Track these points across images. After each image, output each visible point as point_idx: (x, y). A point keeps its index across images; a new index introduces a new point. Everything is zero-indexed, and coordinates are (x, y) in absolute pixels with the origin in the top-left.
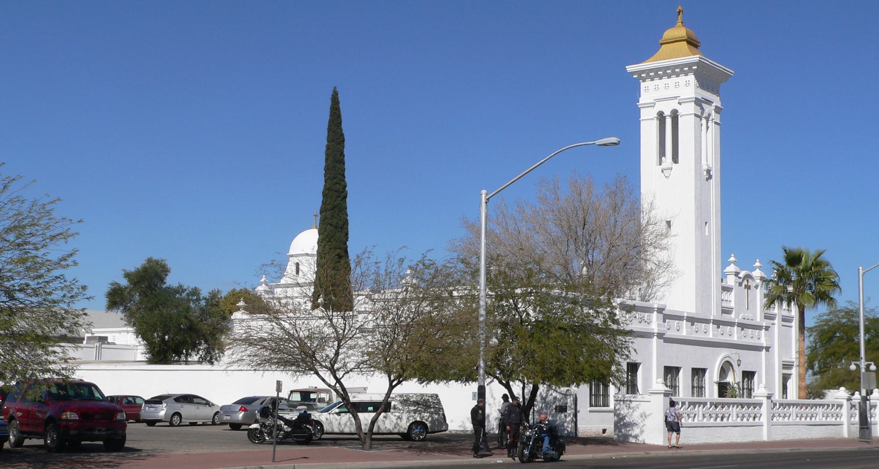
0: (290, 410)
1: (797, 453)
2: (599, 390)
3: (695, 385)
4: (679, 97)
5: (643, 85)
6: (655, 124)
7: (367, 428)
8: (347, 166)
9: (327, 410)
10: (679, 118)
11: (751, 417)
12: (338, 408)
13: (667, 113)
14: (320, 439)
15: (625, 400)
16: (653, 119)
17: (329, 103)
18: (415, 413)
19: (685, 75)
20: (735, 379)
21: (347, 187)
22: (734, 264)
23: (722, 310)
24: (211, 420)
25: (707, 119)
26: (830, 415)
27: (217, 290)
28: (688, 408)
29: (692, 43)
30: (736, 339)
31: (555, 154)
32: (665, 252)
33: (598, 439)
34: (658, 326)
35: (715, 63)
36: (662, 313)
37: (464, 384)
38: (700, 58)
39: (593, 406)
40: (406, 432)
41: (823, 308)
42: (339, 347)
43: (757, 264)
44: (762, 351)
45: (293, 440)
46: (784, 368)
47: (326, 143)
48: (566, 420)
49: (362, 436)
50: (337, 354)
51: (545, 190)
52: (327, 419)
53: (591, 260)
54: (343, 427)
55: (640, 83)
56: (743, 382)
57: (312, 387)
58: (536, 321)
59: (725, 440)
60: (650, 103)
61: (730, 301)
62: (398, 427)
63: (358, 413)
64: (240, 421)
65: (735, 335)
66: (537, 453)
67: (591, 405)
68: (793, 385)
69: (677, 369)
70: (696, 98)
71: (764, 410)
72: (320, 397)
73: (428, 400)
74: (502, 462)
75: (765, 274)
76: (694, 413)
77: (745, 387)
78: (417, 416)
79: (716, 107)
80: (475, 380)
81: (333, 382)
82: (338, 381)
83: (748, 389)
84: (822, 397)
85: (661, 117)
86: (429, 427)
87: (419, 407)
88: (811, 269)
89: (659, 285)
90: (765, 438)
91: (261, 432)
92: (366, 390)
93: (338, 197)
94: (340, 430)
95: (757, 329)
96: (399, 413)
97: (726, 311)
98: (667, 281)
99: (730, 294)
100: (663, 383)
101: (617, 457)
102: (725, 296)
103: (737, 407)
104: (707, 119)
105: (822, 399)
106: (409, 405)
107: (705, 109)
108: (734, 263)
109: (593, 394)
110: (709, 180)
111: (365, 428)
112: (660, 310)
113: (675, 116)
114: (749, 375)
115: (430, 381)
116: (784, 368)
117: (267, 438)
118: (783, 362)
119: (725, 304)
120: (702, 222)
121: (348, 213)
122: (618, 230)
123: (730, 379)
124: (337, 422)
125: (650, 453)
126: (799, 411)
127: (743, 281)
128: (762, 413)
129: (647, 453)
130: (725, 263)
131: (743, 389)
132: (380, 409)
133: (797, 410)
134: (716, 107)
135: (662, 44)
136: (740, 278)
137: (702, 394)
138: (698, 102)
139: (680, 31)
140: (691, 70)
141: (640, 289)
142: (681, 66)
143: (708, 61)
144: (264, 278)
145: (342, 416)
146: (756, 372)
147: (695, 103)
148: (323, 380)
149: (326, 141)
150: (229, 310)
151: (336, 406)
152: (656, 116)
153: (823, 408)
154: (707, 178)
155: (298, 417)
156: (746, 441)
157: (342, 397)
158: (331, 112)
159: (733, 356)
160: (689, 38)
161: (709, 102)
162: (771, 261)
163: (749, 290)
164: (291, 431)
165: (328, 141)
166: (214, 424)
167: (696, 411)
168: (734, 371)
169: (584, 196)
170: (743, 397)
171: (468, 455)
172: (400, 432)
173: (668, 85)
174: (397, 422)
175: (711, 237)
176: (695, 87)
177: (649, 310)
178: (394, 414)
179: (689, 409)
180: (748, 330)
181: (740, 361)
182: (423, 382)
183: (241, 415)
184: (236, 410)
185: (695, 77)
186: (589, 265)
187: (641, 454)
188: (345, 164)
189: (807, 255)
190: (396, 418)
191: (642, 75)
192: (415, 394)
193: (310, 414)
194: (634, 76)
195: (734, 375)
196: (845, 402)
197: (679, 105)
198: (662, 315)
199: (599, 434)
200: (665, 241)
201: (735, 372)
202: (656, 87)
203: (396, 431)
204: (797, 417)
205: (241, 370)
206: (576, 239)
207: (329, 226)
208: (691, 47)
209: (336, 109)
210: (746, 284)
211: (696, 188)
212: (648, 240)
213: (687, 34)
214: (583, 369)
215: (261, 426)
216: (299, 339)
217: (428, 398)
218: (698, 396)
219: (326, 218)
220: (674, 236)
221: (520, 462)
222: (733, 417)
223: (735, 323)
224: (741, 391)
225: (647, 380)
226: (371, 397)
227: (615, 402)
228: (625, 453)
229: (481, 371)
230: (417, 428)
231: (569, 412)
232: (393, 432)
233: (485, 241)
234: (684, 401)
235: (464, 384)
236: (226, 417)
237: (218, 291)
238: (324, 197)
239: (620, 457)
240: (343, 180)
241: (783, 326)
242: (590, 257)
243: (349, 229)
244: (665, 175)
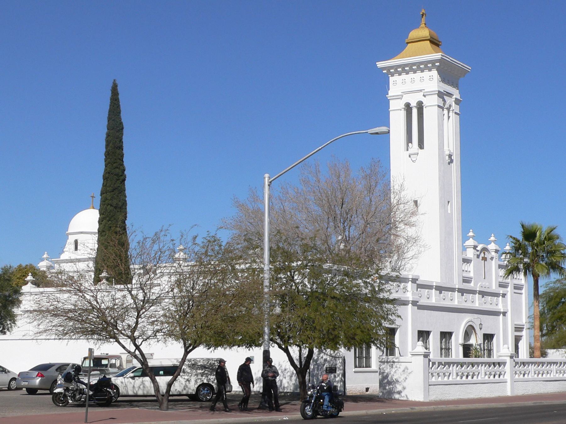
0: (85, 375)
1: (539, 406)
2: (362, 353)
3: (443, 347)
4: (424, 90)
5: (392, 79)
6: (402, 114)
7: (165, 391)
8: (125, 151)
9: (122, 375)
10: (424, 109)
11: (492, 375)
12: (132, 372)
13: (413, 104)
14: (116, 401)
15: (389, 361)
16: (401, 110)
17: (109, 94)
18: (202, 376)
19: (429, 71)
20: (477, 341)
21: (126, 170)
22: (473, 239)
23: (463, 279)
24: (7, 386)
25: (448, 109)
26: (545, 372)
27: (9, 266)
28: (438, 368)
29: (435, 42)
30: (477, 305)
31: (331, 142)
32: (414, 228)
33: (366, 397)
34: (412, 295)
35: (455, 60)
36: (416, 283)
37: (248, 349)
38: (442, 55)
39: (357, 367)
40: (194, 393)
41: (555, 276)
42: (138, 316)
43: (492, 238)
44: (500, 316)
45: (94, 403)
46: (516, 331)
47: (106, 130)
48: (335, 380)
49: (160, 397)
50: (137, 323)
51: (307, 173)
52: (122, 383)
53: (347, 236)
54: (137, 389)
55: (389, 77)
56: (484, 344)
57: (104, 354)
58: (312, 292)
59: (476, 396)
60: (398, 96)
61: (470, 272)
62: (187, 389)
63: (156, 377)
64: (37, 386)
65: (477, 302)
66: (319, 411)
67: (356, 367)
68: (523, 346)
69: (428, 333)
70: (439, 91)
71: (508, 368)
72: (111, 363)
73: (214, 364)
74: (288, 419)
75: (499, 248)
76: (449, 372)
77: (486, 348)
78: (205, 379)
79: (456, 99)
80: (259, 345)
81: (132, 348)
82: (137, 347)
83: (488, 350)
84: (544, 356)
85: (408, 108)
86: (215, 388)
87: (205, 371)
88: (544, 243)
89: (408, 258)
90: (508, 393)
91: (65, 396)
92: (152, 356)
93: (117, 180)
94: (134, 393)
95: (495, 296)
96: (188, 376)
97: (467, 280)
98: (414, 255)
99: (469, 265)
100: (422, 346)
101: (387, 412)
102: (465, 267)
103: (485, 366)
104: (448, 109)
105: (544, 357)
106: (197, 369)
107: (446, 101)
108: (473, 237)
109: (357, 356)
110: (451, 164)
111: (163, 388)
112: (414, 281)
113: (420, 107)
114: (488, 337)
115: (218, 347)
116: (516, 331)
117: (70, 401)
118: (515, 325)
119: (465, 275)
120: (446, 202)
121: (126, 195)
122: (373, 209)
123: (473, 341)
124: (132, 386)
125: (415, 409)
126: (537, 369)
127: (480, 253)
128: (506, 371)
129: (412, 409)
130: (465, 238)
131: (484, 350)
132: (176, 372)
133: (535, 368)
134: (456, 99)
135: (408, 43)
136: (478, 251)
137: (449, 355)
138: (441, 95)
139: (424, 32)
140: (434, 66)
141: (391, 262)
142: (426, 63)
143: (449, 59)
144: (46, 255)
145: (136, 380)
146: (494, 334)
147: (438, 96)
148: (124, 347)
149: (106, 129)
150: (16, 284)
151: (131, 371)
152: (404, 107)
153: (556, 365)
154: (449, 162)
155: (98, 381)
156: (493, 396)
157: (141, 362)
158: (111, 103)
159: (475, 321)
160: (432, 38)
161: (450, 95)
162: (508, 236)
163: (485, 262)
164: (92, 394)
165: (108, 129)
166: (9, 389)
167: (451, 370)
168: (476, 334)
169: (342, 178)
170: (484, 357)
171: (256, 413)
172: (189, 393)
173: (414, 80)
174: (186, 384)
175: (452, 215)
176: (438, 82)
177: (405, 280)
178: (183, 377)
179: (439, 369)
180: (469, 294)
181: (482, 325)
182: (210, 348)
183: (38, 381)
184: (34, 376)
185: (438, 72)
186: (346, 241)
187: (407, 409)
188: (124, 150)
189: (540, 229)
190: (185, 380)
191: (391, 71)
192: (202, 359)
193: (110, 379)
194: (384, 72)
195: (476, 338)
196: (508, 360)
197: (423, 97)
198: (416, 284)
199: (363, 392)
200: (413, 219)
201: (477, 335)
202: (404, 81)
203: (184, 392)
204: (535, 373)
205: (49, 339)
206: (335, 217)
207: (109, 206)
208: (434, 45)
209: (116, 100)
210: (483, 256)
211: (440, 171)
212: (400, 218)
213: (429, 35)
214: (355, 334)
215: (65, 390)
216: (99, 310)
217: (214, 362)
218: (446, 356)
219: (107, 199)
220: (422, 214)
221: (303, 419)
222: (453, 376)
223: (477, 291)
224: (482, 352)
225: (404, 341)
226: (161, 362)
227: (380, 363)
228: (394, 409)
229: (266, 337)
230: (204, 389)
231: (338, 372)
232: (182, 393)
233: (269, 219)
234: (434, 361)
235: (248, 349)
236: (24, 383)
237: (10, 267)
238: (104, 179)
239: (390, 412)
240: (122, 165)
241: (515, 293)
242: (347, 233)
243: (127, 209)
244: (412, 160)
